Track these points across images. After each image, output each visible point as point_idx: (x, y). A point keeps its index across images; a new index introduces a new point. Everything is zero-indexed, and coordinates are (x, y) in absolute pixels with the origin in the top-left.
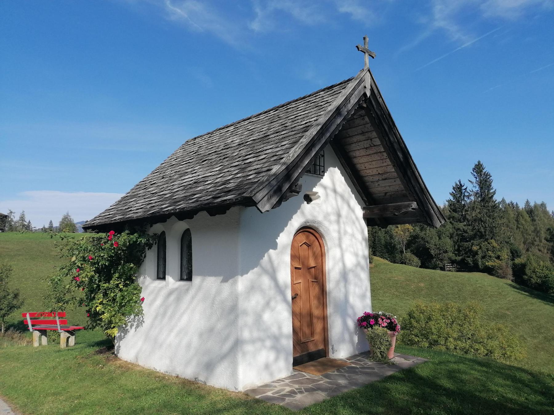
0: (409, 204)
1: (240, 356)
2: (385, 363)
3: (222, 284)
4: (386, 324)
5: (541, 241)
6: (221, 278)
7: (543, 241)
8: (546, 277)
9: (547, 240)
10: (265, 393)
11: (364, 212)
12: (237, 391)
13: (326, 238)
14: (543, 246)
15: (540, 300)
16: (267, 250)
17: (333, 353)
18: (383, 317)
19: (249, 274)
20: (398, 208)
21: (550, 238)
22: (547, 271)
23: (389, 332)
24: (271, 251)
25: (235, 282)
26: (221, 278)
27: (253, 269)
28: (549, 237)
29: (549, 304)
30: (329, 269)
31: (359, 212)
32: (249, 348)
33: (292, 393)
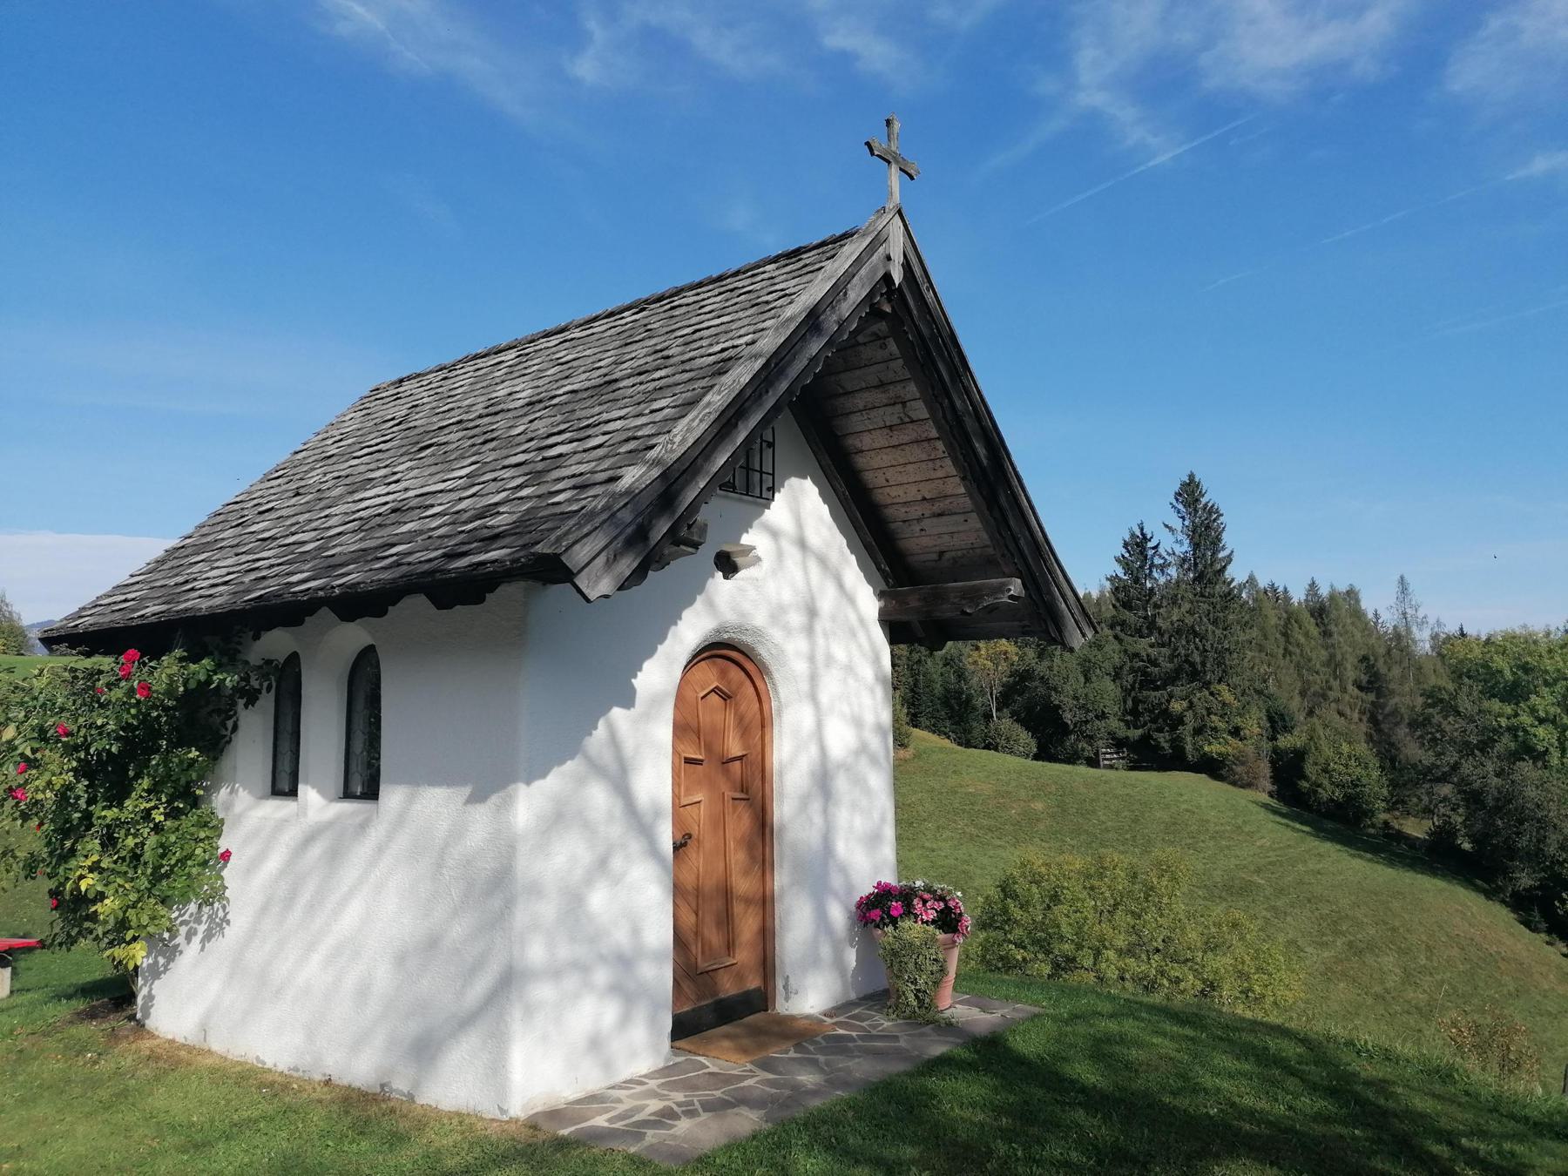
0: (1004, 584)
1: (517, 1013)
3: (470, 808)
4: (932, 915)
5: (1344, 690)
7: (1350, 687)
9: (1360, 688)
11: (882, 603)
17: (787, 999)
20: (973, 595)
21: (1369, 682)
23: (941, 936)
24: (617, 713)
25: (507, 804)
27: (561, 762)
28: (1364, 678)
29: (1361, 857)
31: (868, 603)
32: (543, 992)
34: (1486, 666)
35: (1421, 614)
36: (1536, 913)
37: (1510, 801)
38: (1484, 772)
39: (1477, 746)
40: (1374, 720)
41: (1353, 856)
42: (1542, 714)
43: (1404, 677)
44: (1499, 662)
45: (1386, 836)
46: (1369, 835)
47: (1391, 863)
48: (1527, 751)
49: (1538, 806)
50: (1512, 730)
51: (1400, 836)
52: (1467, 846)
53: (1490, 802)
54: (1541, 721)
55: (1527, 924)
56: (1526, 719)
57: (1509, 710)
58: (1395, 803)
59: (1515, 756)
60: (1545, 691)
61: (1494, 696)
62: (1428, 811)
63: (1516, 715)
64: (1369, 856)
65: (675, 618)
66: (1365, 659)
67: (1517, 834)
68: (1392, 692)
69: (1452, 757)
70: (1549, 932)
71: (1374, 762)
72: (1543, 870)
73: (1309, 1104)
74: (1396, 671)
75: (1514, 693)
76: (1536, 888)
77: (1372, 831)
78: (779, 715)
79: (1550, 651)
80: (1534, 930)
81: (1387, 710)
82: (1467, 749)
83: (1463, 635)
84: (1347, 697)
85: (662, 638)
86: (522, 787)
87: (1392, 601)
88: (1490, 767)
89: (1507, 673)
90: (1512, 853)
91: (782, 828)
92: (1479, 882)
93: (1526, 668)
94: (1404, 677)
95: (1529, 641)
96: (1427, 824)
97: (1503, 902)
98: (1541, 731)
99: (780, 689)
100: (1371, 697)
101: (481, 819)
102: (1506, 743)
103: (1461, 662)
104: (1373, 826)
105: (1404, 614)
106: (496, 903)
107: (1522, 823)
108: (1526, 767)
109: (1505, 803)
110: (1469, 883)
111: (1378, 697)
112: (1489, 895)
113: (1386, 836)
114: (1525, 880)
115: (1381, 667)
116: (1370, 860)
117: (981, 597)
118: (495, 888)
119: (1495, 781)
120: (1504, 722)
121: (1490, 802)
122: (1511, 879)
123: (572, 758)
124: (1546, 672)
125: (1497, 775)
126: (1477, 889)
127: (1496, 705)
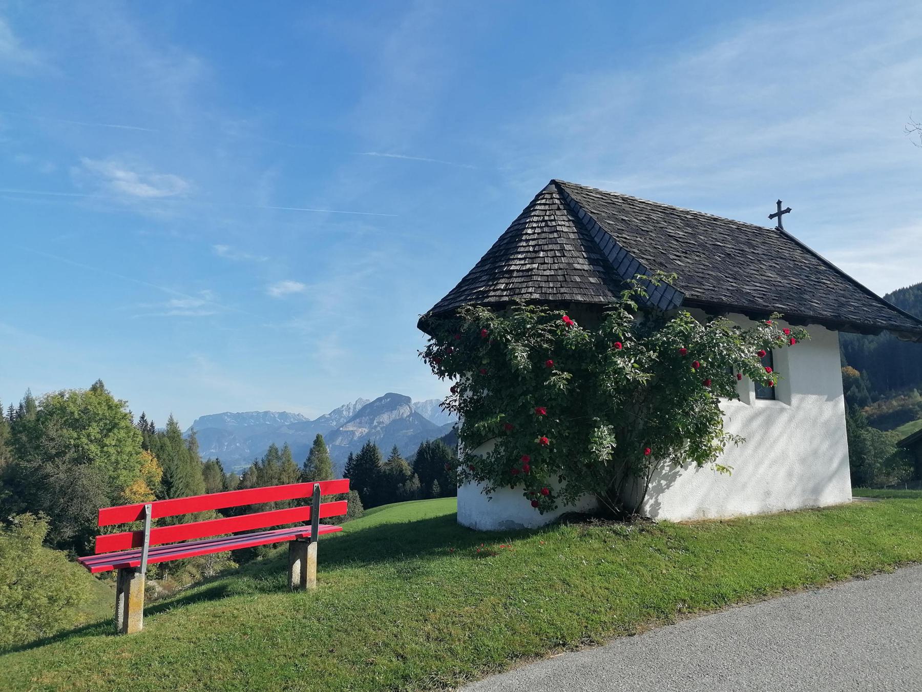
26: (826, 397)
44: (72, 408)
56: (84, 440)
59: (77, 461)
60: (95, 424)
75: (76, 424)
88: (63, 468)
89: (76, 414)
102: (71, 454)
120: (72, 442)
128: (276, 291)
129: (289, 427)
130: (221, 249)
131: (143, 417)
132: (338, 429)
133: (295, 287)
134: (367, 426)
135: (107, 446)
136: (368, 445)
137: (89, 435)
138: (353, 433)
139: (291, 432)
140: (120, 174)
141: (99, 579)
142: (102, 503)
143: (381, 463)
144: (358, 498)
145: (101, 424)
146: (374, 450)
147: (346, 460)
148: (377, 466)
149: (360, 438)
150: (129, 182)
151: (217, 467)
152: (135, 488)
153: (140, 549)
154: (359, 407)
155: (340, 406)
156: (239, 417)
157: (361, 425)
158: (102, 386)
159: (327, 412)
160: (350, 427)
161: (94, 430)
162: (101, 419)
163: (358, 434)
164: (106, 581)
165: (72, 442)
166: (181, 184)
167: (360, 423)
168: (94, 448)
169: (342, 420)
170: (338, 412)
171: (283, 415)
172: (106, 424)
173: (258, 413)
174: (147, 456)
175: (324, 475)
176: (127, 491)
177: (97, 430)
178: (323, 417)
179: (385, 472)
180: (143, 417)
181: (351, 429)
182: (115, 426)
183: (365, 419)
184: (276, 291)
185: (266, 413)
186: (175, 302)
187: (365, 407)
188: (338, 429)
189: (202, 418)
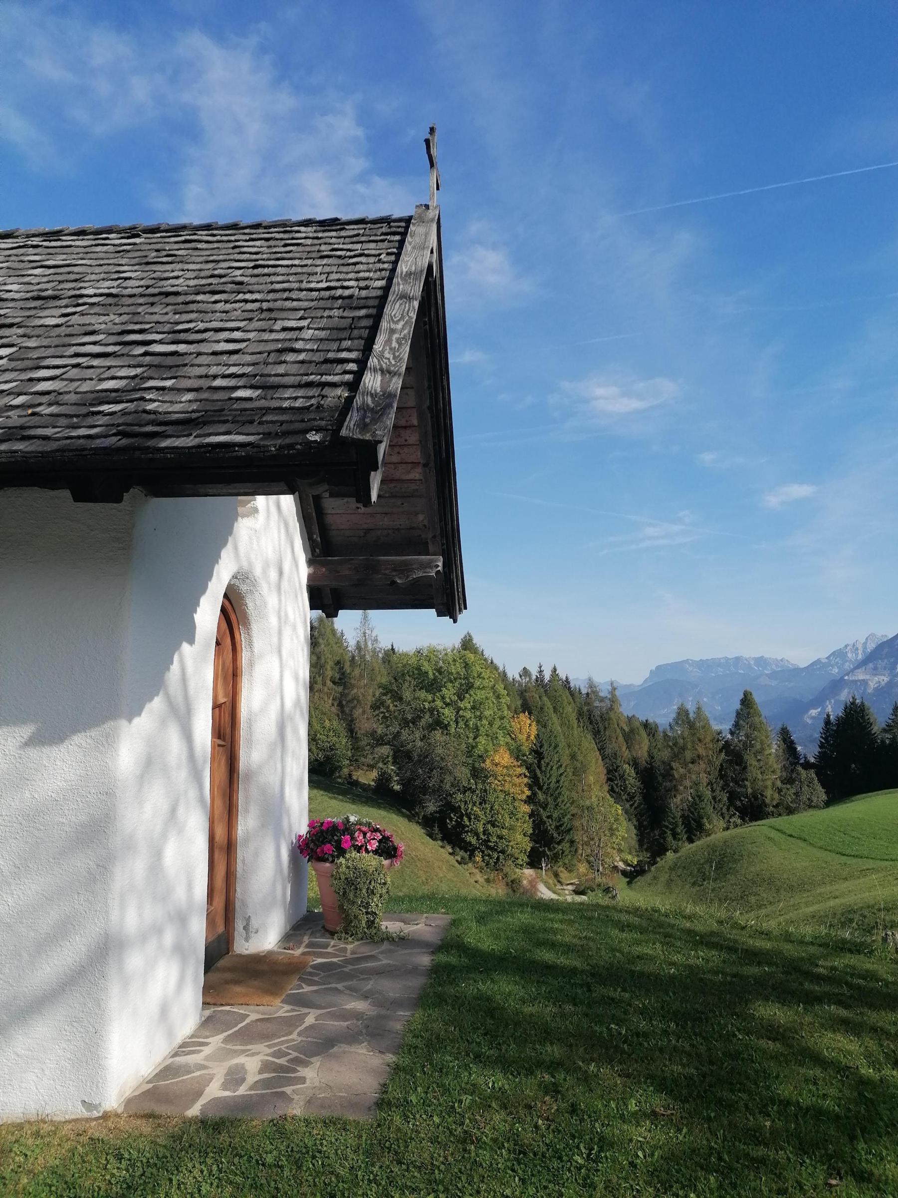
0: (432, 561)
1: (114, 989)
2: (383, 940)
3: (33, 753)
4: (375, 845)
5: (324, 684)
6: (26, 731)
7: (329, 683)
8: (332, 750)
9: (334, 683)
10: (199, 1094)
11: (311, 570)
12: (96, 1114)
13: (255, 627)
14: (327, 693)
15: (322, 792)
16: (177, 647)
17: (247, 939)
18: (364, 829)
19: (143, 714)
20: (404, 568)
21: (340, 679)
22: (335, 738)
23: (386, 862)
24: (185, 646)
25: (110, 741)
26: (26, 731)
27: (151, 699)
28: (337, 676)
29: (335, 798)
30: (250, 712)
31: (304, 571)
32: (134, 961)
33: (280, 1074)
34: (419, 668)
35: (374, 635)
36: (436, 828)
37: (426, 757)
38: (413, 738)
39: (410, 721)
40: (340, 705)
41: (331, 798)
42: (448, 700)
43: (361, 676)
44: (426, 667)
45: (349, 783)
46: (339, 783)
47: (353, 802)
48: (438, 724)
49: (442, 758)
50: (431, 710)
51: (356, 783)
52: (397, 788)
53: (416, 758)
54: (447, 705)
55: (431, 836)
56: (439, 703)
57: (430, 697)
58: (354, 760)
59: (431, 727)
60: (449, 685)
61: (422, 688)
62: (371, 767)
63: (434, 701)
64: (341, 797)
65: (216, 558)
66: (338, 663)
67: (429, 777)
68: (353, 686)
69: (395, 729)
70: (442, 840)
71: (344, 733)
72: (441, 800)
73: (715, 957)
74: (357, 672)
75: (433, 686)
76: (436, 812)
77: (339, 780)
78: (251, 664)
79: (454, 660)
80: (435, 839)
81: (350, 697)
82: (405, 723)
83: (393, 649)
84: (326, 689)
85: (210, 576)
86: (123, 723)
87: (358, 625)
88: (418, 735)
89: (430, 673)
90: (425, 790)
91: (249, 776)
92: (404, 811)
93: (439, 670)
94: (361, 676)
95: (433, 651)
96: (374, 774)
97: (418, 822)
98: (446, 711)
99: (255, 640)
100: (340, 689)
101: (61, 767)
102: (427, 719)
103: (404, 666)
104: (340, 777)
105: (365, 633)
106: (81, 863)
107: (432, 771)
108: (438, 735)
109: (426, 760)
110: (400, 813)
111: (344, 689)
112: (410, 818)
113: (349, 783)
114: (431, 807)
115: (347, 668)
116: (342, 801)
117: (412, 570)
118: (278, 833)
119: (419, 744)
120: (427, 705)
121: (416, 758)
122: (423, 807)
123: (157, 694)
124: (452, 673)
125: (421, 740)
126: (404, 815)
127: (423, 694)
128: (773, 501)
129: (770, 676)
130: (708, 457)
131: (555, 670)
132: (842, 678)
133: (799, 491)
134: (887, 672)
135: (461, 709)
136: (853, 703)
137: (443, 698)
138: (865, 682)
139: (774, 683)
140: (600, 391)
141: (460, 863)
142: (463, 773)
143: (876, 729)
144: (816, 781)
145: (457, 684)
146: (863, 710)
147: (822, 725)
148: (869, 733)
149: (876, 689)
150: (610, 398)
151: (643, 733)
152: (497, 759)
153: (821, 794)
154: (871, 646)
155: (842, 646)
156: (704, 665)
157: (875, 671)
158: (471, 640)
159: (823, 655)
160: (860, 676)
161: (449, 692)
162: (455, 679)
163: (872, 685)
164: (466, 867)
165: (427, 705)
166: (668, 388)
167: (875, 669)
168: (448, 713)
169: (848, 666)
170: (839, 654)
171: (761, 661)
172: (461, 685)
173: (727, 659)
174: (524, 718)
175: (758, 746)
176: (488, 761)
177: (453, 691)
178: (818, 661)
179: (883, 742)
180: (555, 670)
181: (861, 677)
182: (470, 686)
183: (880, 664)
184: (773, 501)
185: (738, 659)
186: (650, 531)
187: (881, 646)
188: (842, 678)
189: (659, 668)
